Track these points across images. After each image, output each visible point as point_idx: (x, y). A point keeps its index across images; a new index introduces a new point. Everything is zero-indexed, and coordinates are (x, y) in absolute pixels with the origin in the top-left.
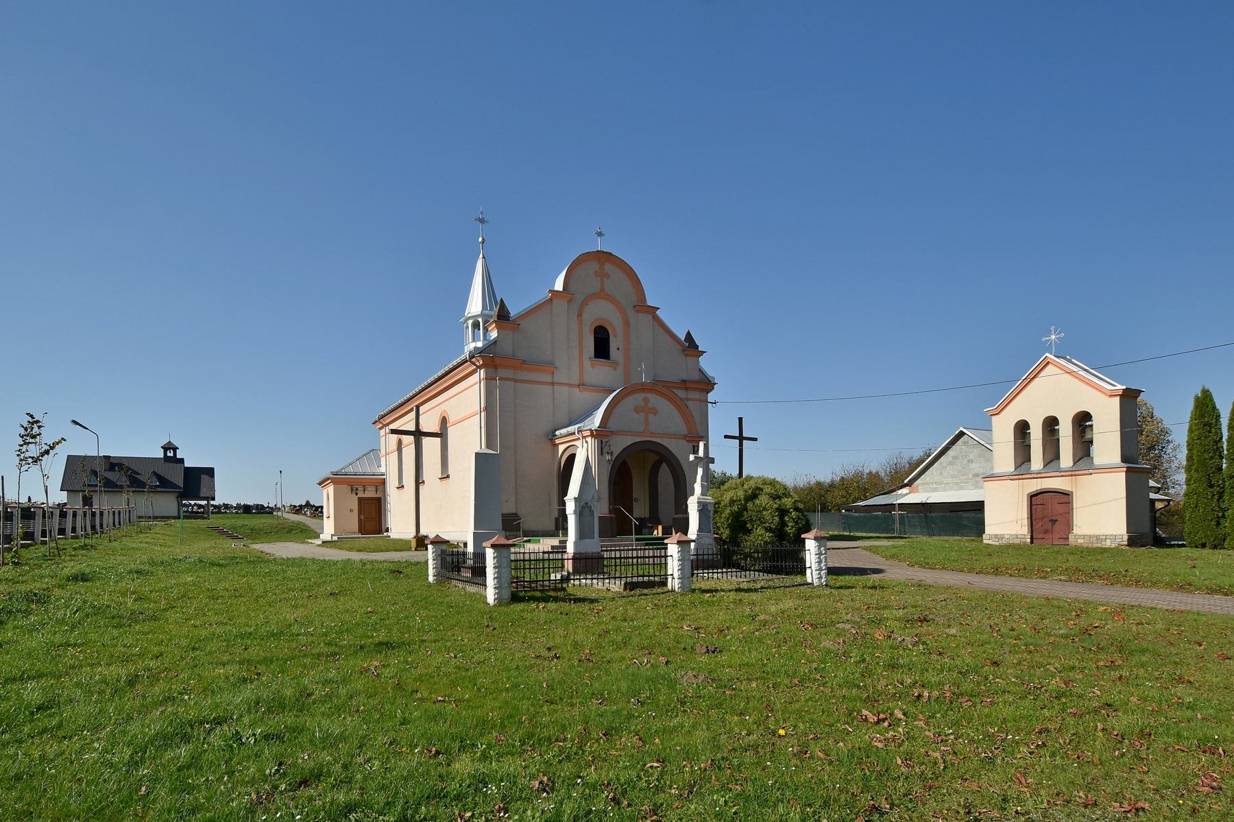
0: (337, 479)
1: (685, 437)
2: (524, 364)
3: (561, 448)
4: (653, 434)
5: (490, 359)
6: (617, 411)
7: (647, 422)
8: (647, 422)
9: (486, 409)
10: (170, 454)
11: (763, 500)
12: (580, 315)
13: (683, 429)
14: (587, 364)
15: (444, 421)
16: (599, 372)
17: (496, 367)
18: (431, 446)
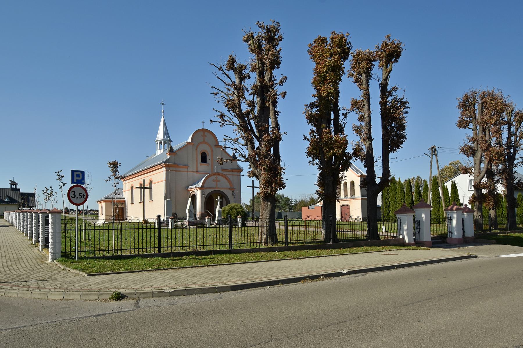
0: (107, 200)
1: (229, 189)
2: (179, 166)
3: (190, 192)
4: (219, 188)
5: (168, 165)
6: (207, 181)
7: (217, 184)
8: (217, 184)
9: (166, 180)
10: (14, 187)
11: (234, 210)
12: (196, 149)
13: (228, 186)
14: (199, 165)
15: (151, 182)
16: (203, 167)
17: (169, 167)
18: (147, 191)
